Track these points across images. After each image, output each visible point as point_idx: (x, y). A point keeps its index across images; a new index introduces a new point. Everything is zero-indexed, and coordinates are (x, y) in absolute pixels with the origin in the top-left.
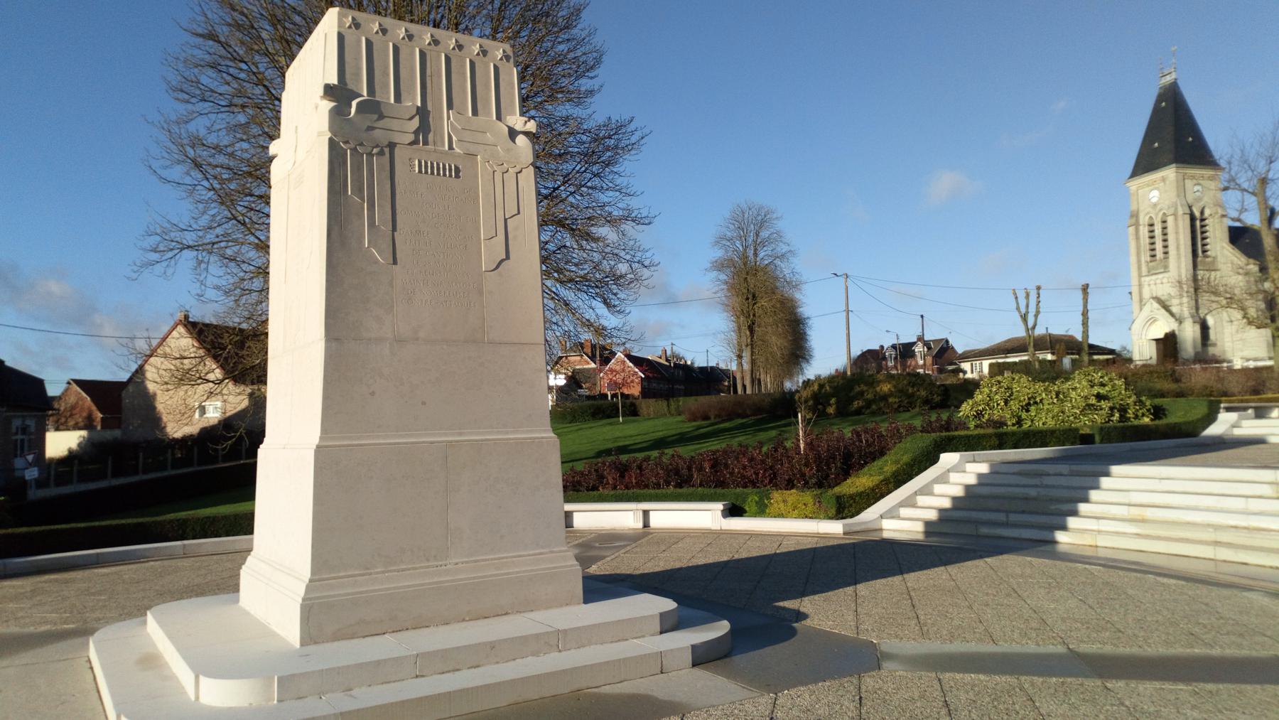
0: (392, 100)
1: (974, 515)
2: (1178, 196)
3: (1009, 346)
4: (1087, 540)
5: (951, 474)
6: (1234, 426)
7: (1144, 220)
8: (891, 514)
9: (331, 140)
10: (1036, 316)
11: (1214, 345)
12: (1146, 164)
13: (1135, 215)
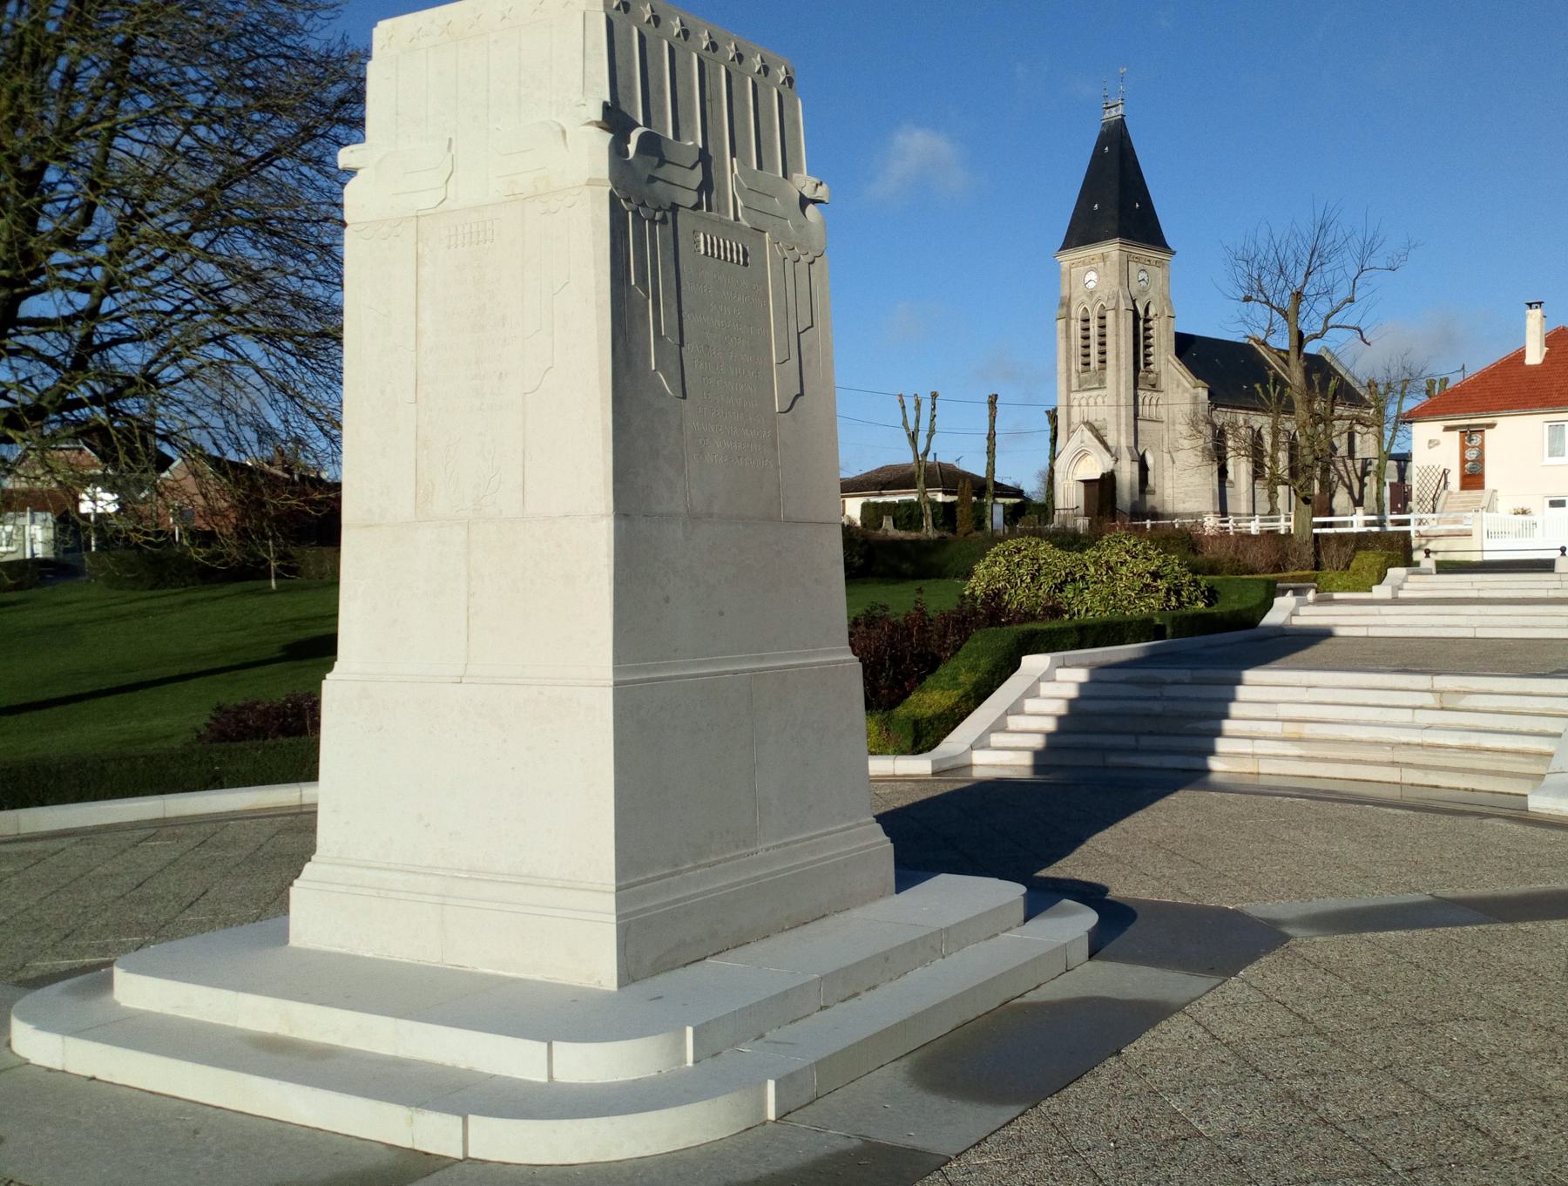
0: (670, 135)
1: (1095, 739)
2: (1121, 284)
3: (883, 477)
4: (1248, 767)
5: (1042, 685)
6: (1293, 615)
7: (1076, 312)
8: (981, 743)
9: (611, 193)
10: (930, 437)
11: (1153, 492)
12: (1081, 233)
13: (1066, 304)
